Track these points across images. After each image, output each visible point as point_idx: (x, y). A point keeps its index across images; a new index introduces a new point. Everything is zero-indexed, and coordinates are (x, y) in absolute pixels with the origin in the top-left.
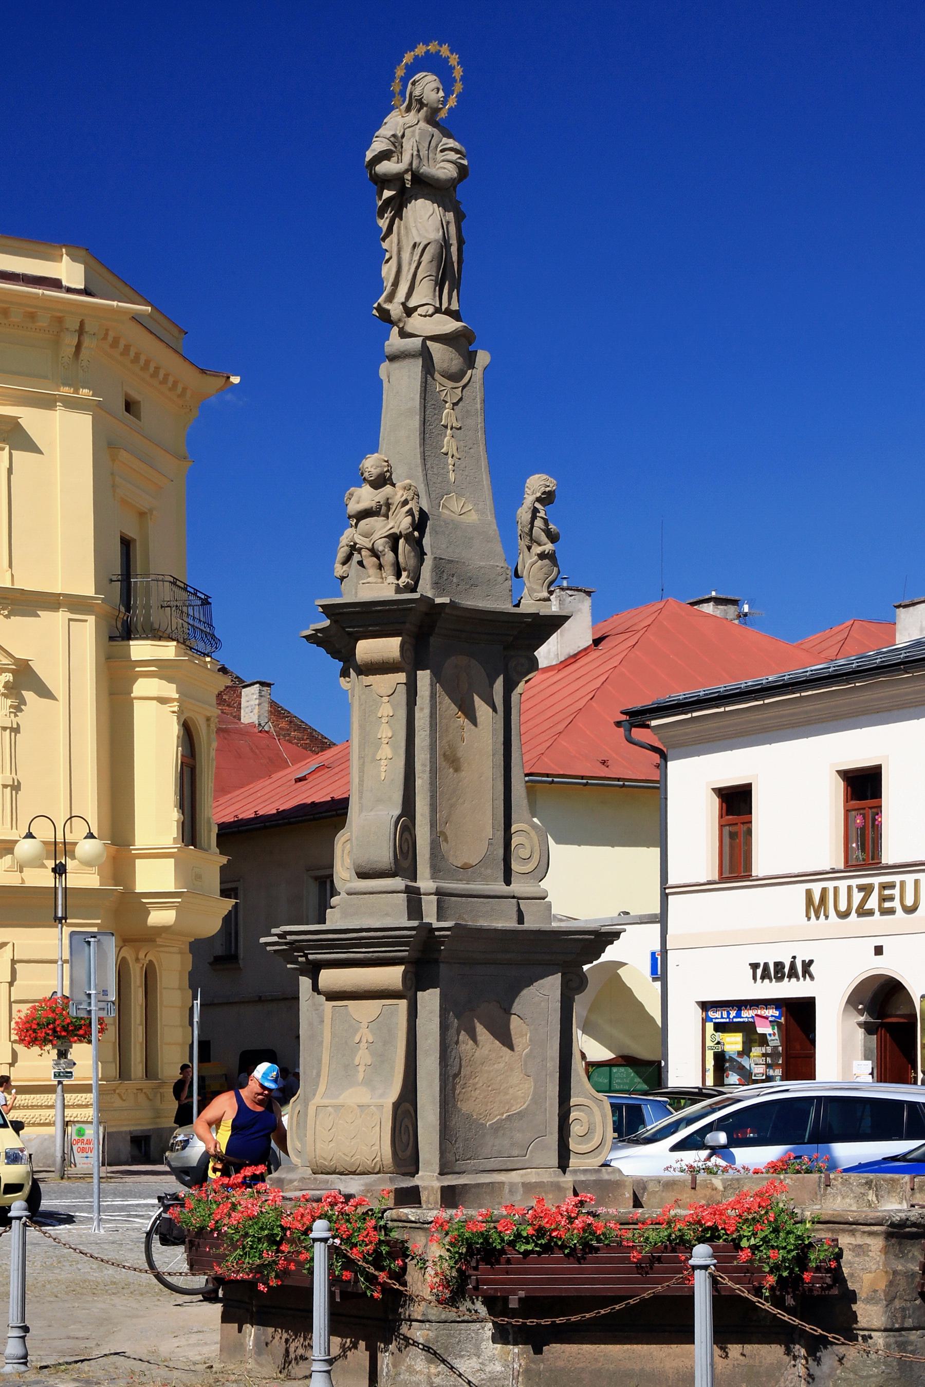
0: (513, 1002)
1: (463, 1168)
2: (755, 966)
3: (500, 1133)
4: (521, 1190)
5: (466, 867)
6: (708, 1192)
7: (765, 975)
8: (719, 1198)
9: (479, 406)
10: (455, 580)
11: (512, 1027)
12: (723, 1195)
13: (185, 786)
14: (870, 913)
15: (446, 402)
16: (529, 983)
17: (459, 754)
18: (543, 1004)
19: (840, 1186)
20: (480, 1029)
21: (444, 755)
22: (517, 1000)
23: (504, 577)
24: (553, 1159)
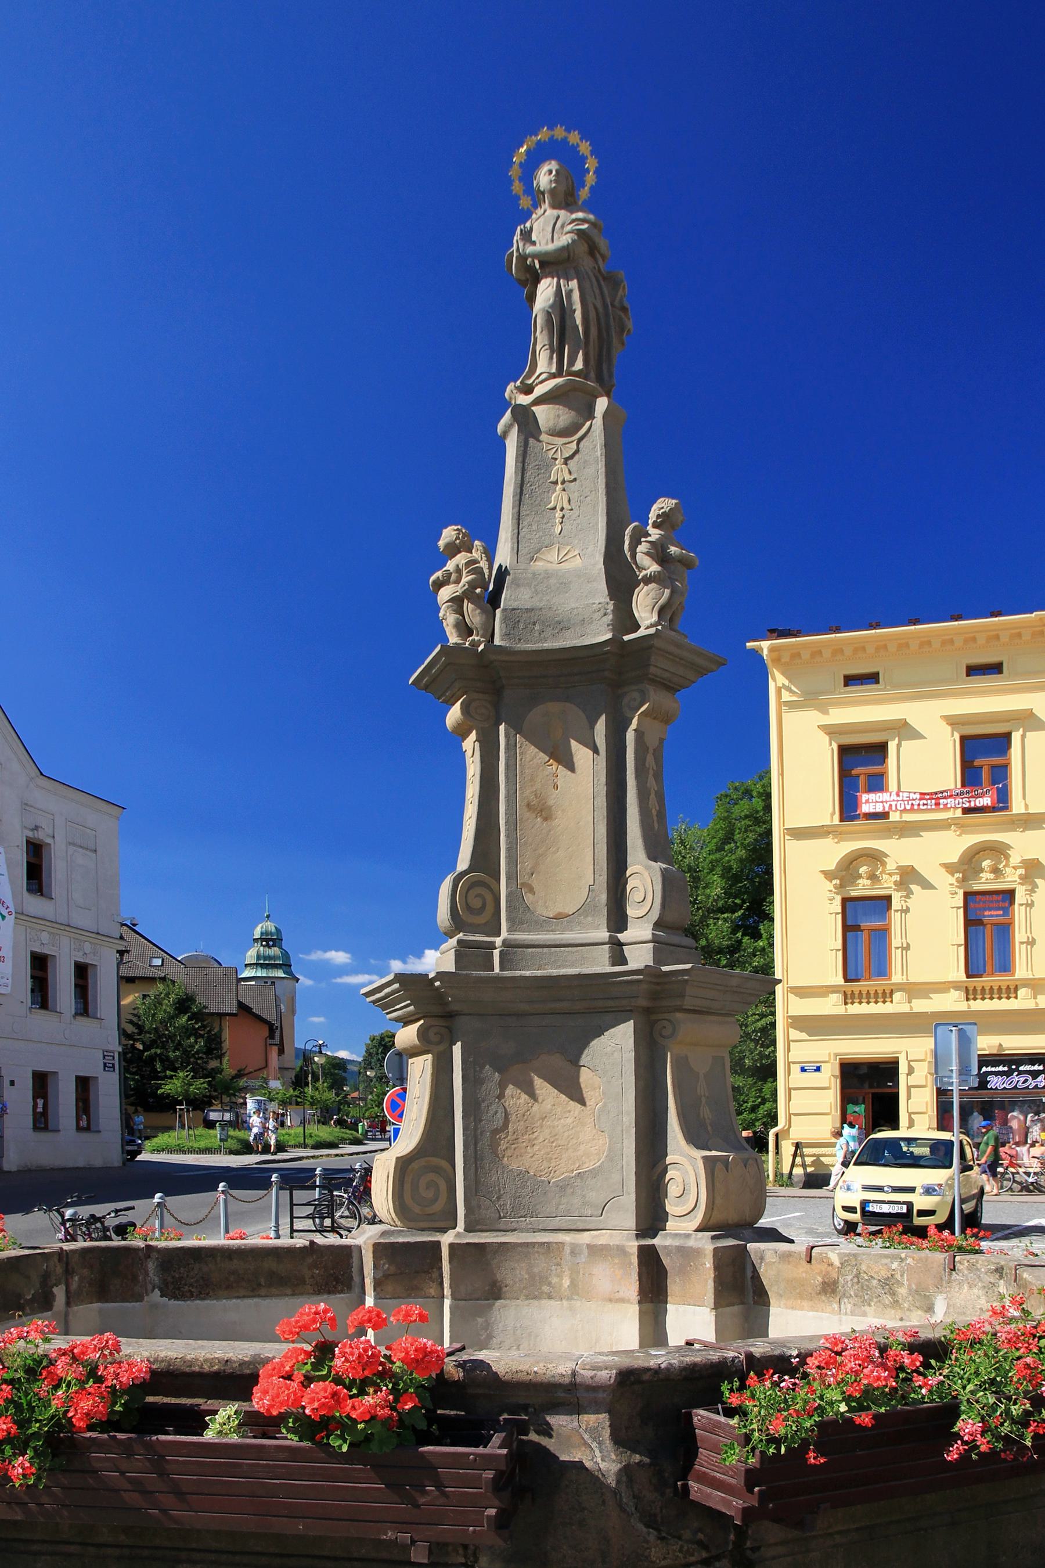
0: (581, 1053)
1: (514, 1225)
3: (569, 1191)
4: (586, 1251)
5: (558, 917)
6: (824, 1267)
8: (835, 1276)
9: (599, 453)
10: (537, 627)
11: (581, 1080)
12: (839, 1272)
14: (286, 955)
15: (556, 459)
16: (600, 1033)
17: (551, 802)
18: (616, 1054)
19: (966, 1272)
20: (538, 1082)
21: (528, 805)
22: (586, 1051)
23: (602, 612)
24: (629, 1220)
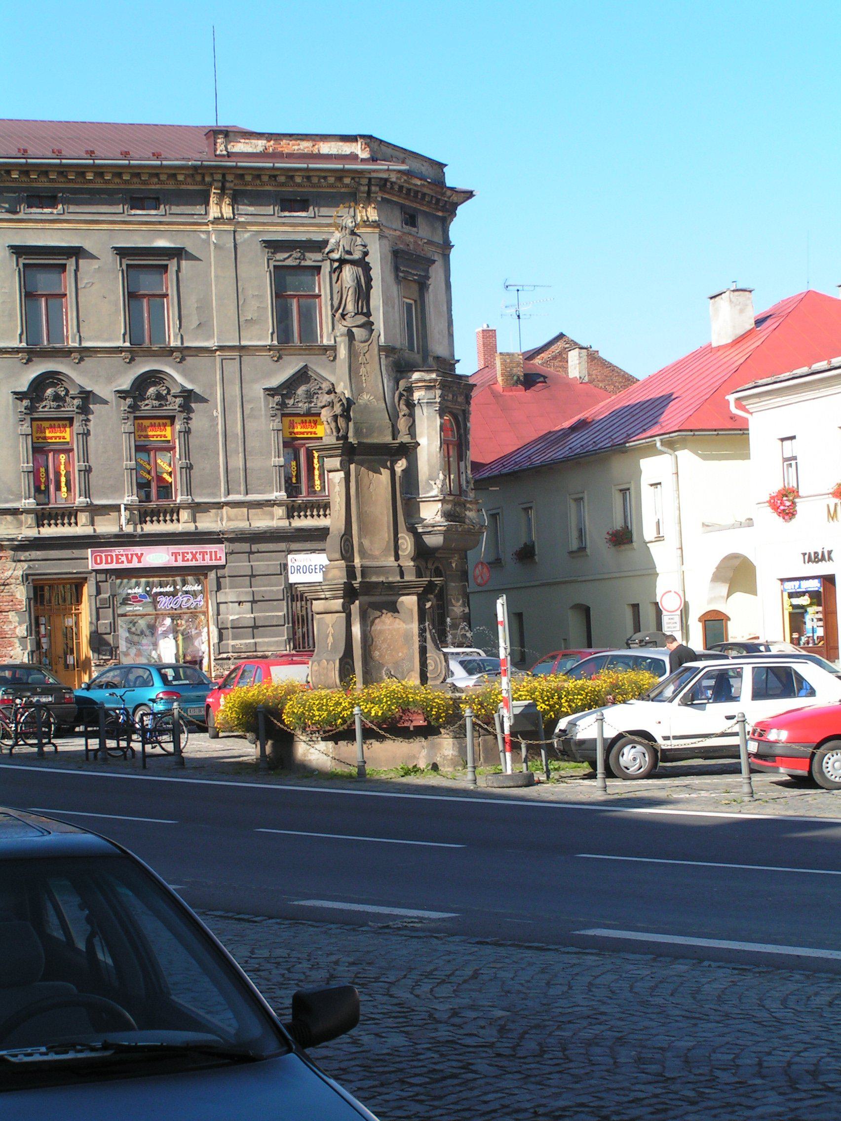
2: (804, 554)
7: (810, 560)
13: (102, 211)
